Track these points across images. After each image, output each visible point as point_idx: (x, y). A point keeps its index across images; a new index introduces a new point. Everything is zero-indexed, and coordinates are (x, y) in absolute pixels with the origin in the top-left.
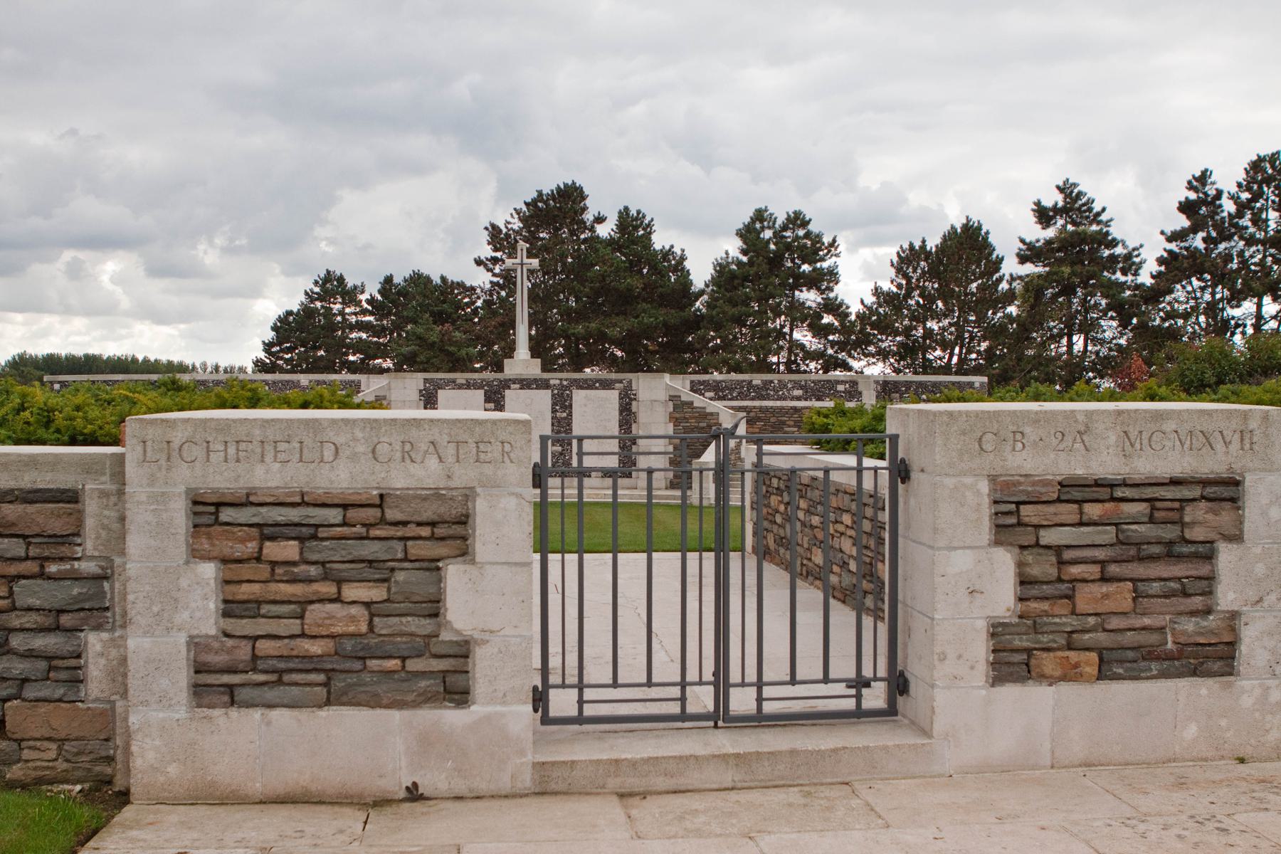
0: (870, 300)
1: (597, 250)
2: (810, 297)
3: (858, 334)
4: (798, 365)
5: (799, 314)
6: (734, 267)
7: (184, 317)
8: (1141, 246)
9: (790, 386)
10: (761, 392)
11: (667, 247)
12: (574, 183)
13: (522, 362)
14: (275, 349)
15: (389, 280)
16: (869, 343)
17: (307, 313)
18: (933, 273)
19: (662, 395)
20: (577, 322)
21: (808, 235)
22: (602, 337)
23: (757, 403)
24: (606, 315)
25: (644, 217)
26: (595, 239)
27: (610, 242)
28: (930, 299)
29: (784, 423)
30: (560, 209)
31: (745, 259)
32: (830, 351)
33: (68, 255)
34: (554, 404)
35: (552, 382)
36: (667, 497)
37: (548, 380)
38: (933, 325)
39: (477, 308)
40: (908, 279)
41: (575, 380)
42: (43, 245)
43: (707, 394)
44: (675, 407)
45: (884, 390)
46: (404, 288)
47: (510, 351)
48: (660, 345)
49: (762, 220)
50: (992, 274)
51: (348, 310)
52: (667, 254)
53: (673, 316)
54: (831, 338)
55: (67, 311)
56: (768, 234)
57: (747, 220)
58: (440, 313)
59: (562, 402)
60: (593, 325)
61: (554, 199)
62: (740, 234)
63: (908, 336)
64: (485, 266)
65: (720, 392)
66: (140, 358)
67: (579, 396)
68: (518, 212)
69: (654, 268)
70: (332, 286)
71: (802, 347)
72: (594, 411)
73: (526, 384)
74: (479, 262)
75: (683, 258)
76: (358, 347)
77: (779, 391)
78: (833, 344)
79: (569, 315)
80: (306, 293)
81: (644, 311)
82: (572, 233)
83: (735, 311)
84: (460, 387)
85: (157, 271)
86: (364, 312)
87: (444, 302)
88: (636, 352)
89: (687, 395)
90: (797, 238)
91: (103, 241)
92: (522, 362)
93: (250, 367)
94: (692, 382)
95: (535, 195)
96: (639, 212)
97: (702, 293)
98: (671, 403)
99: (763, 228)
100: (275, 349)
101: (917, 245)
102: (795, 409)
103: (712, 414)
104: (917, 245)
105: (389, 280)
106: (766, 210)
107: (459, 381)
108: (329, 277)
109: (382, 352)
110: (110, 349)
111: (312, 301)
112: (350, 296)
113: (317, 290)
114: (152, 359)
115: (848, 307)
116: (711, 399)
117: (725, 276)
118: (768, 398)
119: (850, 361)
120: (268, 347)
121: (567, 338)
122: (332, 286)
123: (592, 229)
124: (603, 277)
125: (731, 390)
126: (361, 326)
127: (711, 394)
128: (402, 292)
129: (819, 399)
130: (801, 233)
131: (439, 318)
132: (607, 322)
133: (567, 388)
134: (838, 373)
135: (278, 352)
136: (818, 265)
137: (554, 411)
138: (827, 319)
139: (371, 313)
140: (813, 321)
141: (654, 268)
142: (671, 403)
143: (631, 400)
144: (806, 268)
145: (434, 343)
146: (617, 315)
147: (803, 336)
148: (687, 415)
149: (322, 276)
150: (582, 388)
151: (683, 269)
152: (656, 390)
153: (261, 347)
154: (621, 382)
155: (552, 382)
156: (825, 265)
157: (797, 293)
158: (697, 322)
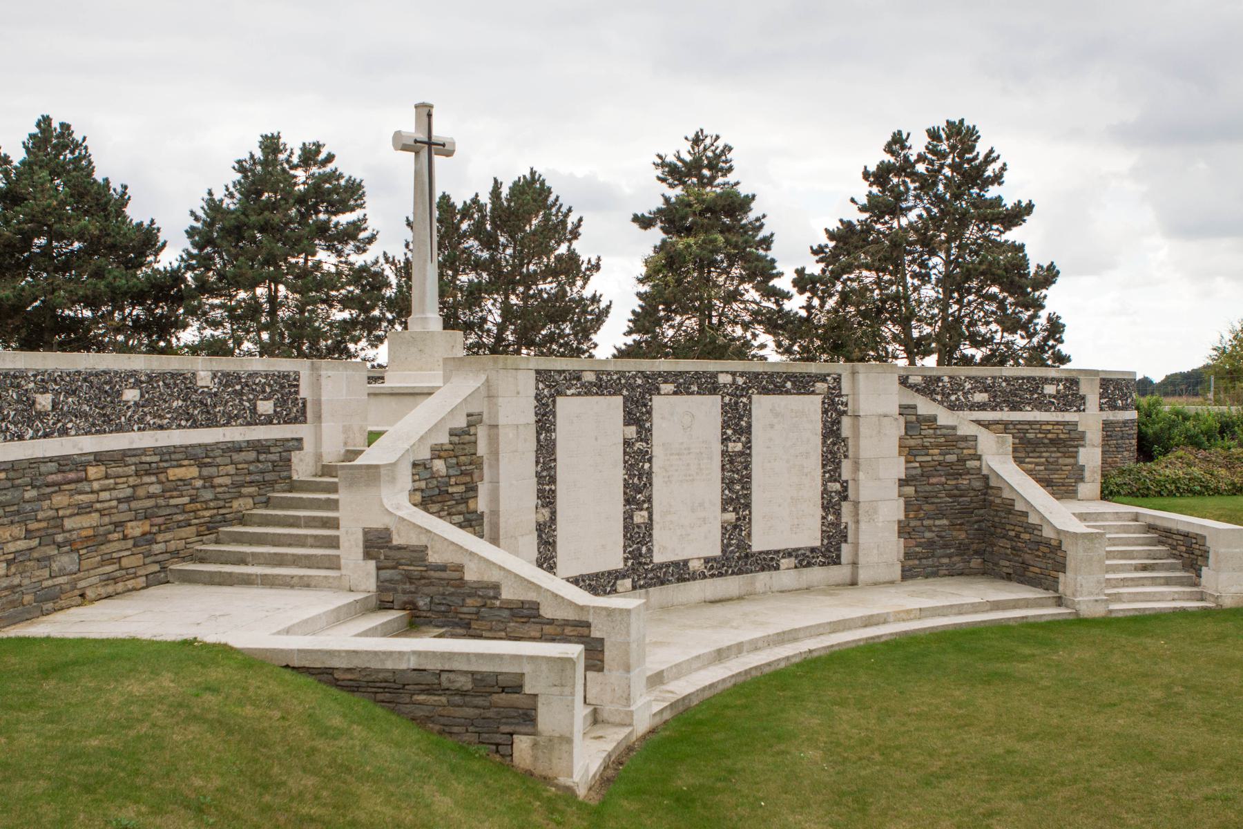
8: (764, 216)
9: (968, 386)
34: (725, 425)
103: (965, 438)
129: (1014, 407)
133: (743, 391)
137: (725, 440)
142: (902, 420)
148: (927, 442)
150: (765, 391)
154: (823, 378)
155: (724, 379)
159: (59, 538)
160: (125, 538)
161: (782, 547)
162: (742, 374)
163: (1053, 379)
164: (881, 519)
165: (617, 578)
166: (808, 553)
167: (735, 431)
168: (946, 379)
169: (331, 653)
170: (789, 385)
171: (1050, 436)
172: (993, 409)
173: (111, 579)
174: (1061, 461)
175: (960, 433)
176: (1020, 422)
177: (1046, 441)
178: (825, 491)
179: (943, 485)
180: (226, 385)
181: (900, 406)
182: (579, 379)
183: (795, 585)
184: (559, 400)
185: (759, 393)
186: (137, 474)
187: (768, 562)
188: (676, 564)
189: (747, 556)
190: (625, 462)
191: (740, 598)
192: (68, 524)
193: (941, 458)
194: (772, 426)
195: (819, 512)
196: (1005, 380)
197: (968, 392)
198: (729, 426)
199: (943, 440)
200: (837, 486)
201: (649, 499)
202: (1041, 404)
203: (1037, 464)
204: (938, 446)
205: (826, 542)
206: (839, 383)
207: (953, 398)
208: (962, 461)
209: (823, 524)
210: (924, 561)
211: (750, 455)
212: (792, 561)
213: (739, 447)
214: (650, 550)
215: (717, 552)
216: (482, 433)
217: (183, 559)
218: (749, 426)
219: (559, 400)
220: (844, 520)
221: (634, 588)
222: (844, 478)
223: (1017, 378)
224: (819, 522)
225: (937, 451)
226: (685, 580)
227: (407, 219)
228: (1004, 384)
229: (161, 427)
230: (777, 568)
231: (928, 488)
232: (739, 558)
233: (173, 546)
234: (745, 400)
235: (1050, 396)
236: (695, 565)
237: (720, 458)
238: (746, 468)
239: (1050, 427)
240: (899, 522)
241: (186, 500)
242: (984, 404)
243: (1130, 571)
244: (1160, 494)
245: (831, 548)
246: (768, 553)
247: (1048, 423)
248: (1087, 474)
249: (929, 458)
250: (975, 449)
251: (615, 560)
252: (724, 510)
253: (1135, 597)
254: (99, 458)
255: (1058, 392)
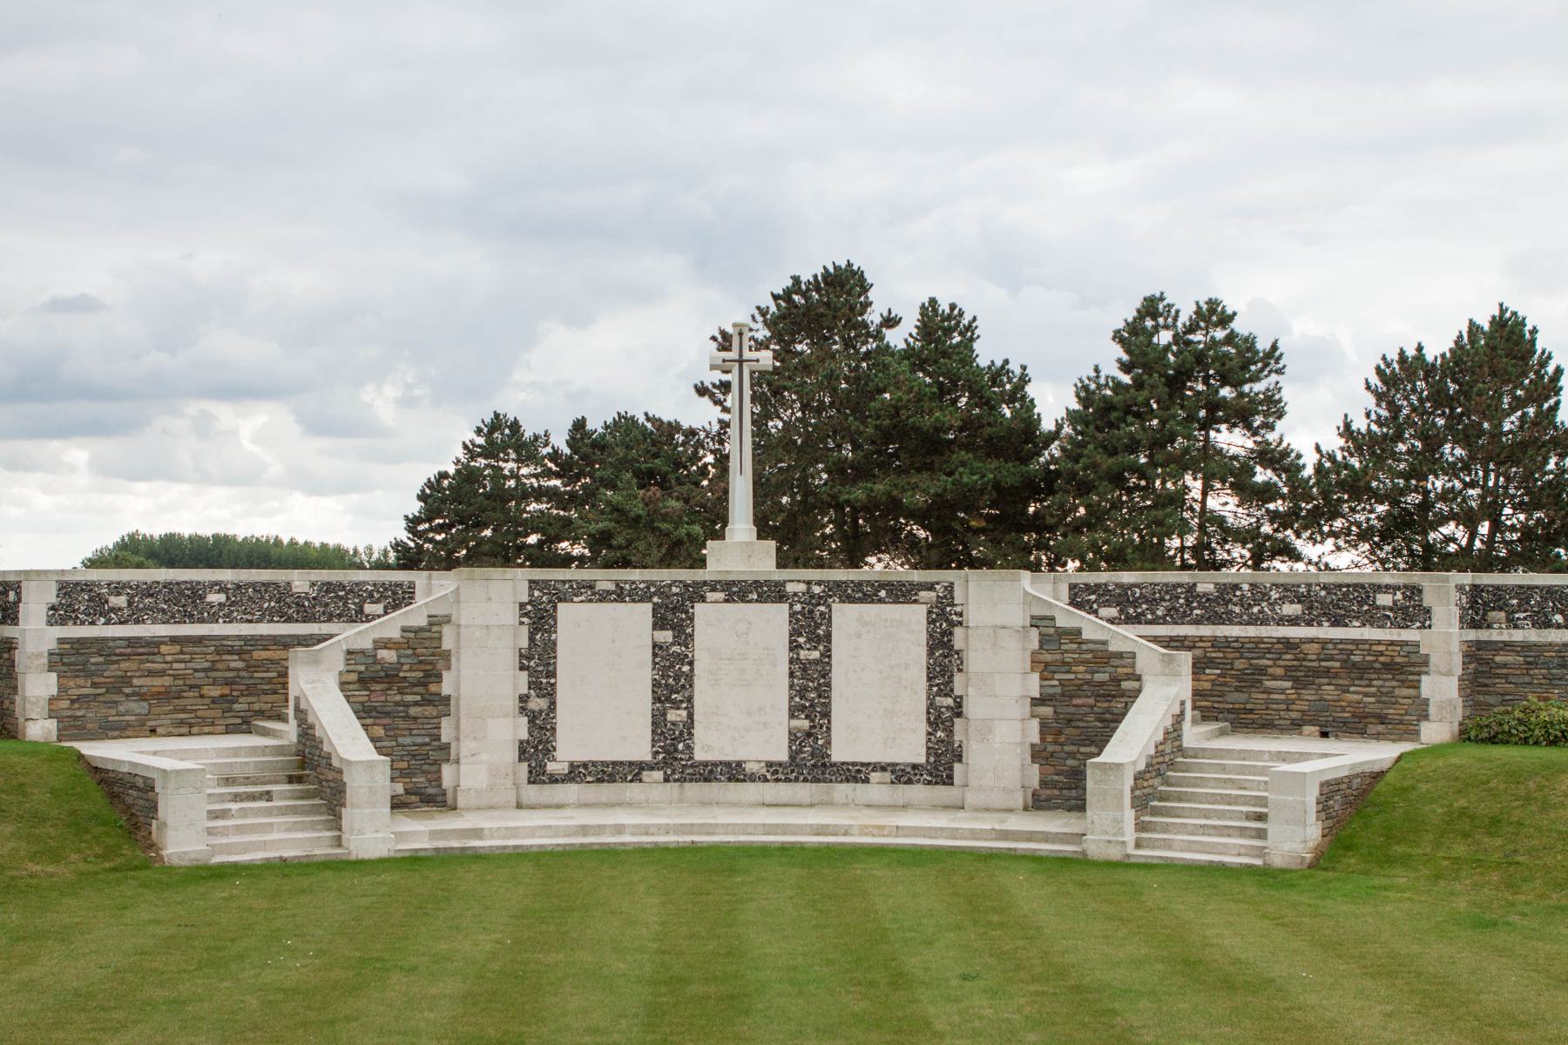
0: (1334, 443)
1: (886, 367)
2: (1232, 440)
3: (1320, 499)
4: (1213, 552)
5: (1217, 469)
6: (1109, 392)
7: (344, 487)
9: (1274, 595)
10: (1218, 607)
11: (999, 363)
12: (849, 264)
13: (741, 549)
14: (421, 528)
15: (579, 425)
16: (1335, 514)
17: (467, 476)
18: (1439, 398)
19: (1018, 617)
20: (854, 482)
21: (1231, 338)
22: (894, 507)
23: (1206, 630)
24: (900, 471)
25: (961, 314)
26: (886, 350)
27: (909, 353)
28: (1432, 442)
29: (1263, 671)
30: (828, 305)
31: (1126, 379)
32: (1267, 529)
33: (193, 408)
34: (794, 633)
35: (790, 588)
36: (1031, 836)
37: (783, 584)
38: (1437, 484)
39: (706, 465)
40: (1395, 409)
41: (838, 584)
42: (164, 392)
43: (1104, 612)
44: (1044, 640)
45: (1473, 603)
46: (602, 436)
47: (715, 519)
48: (988, 518)
49: (1154, 315)
50: (1547, 398)
51: (524, 471)
52: (999, 373)
53: (1010, 473)
54: (1271, 506)
55: (204, 479)
56: (1165, 337)
57: (1131, 315)
58: (651, 474)
59: (811, 628)
60: (880, 487)
61: (818, 289)
62: (1117, 336)
63: (1395, 503)
64: (712, 396)
65: (1130, 607)
66: (286, 541)
67: (845, 616)
68: (763, 312)
69: (980, 397)
70: (502, 436)
71: (1220, 521)
72: (877, 648)
73: (737, 591)
74: (702, 391)
75: (1024, 380)
76: (532, 525)
77: (1254, 606)
78: (1274, 516)
79: (842, 471)
80: (465, 447)
81: (963, 464)
82: (848, 343)
83: (1107, 462)
84: (604, 597)
85: (316, 426)
86: (548, 474)
87: (656, 456)
88: (948, 530)
89: (1068, 617)
90: (1214, 343)
91: (242, 390)
92: (741, 549)
93: (79, 566)
94: (1072, 587)
95: (789, 283)
96: (953, 307)
97: (1055, 436)
98: (1034, 633)
99: (1156, 328)
100: (421, 528)
101: (1411, 352)
102: (1288, 644)
103: (1120, 655)
104: (1411, 352)
105: (579, 425)
106: (1162, 299)
107: (600, 586)
108: (497, 423)
109: (565, 529)
110: (246, 526)
111: (472, 458)
112: (526, 450)
113: (480, 441)
114: (301, 541)
115: (1299, 456)
116: (1111, 621)
117: (1100, 411)
118: (1228, 619)
119: (1299, 544)
120: (412, 523)
121: (839, 507)
122: (502, 436)
123: (878, 336)
124: (896, 409)
125: (1153, 603)
126: (539, 494)
127: (1113, 612)
128: (600, 445)
129: (1337, 622)
130: (1220, 334)
131: (646, 478)
132: (902, 481)
133: (822, 599)
134: (1281, 566)
135: (426, 531)
136: (1246, 388)
137: (794, 647)
138: (1262, 475)
139: (558, 475)
140: (1238, 477)
141: (980, 397)
142: (1034, 633)
143: (952, 624)
144: (1226, 392)
145: (639, 517)
146: (919, 471)
147: (1224, 503)
148: (1068, 658)
149: (488, 421)
150: (850, 599)
151: (1024, 397)
152: (1004, 605)
153: (403, 524)
154: (930, 587)
155: (790, 588)
156: (1259, 387)
157: (1212, 434)
158: (1047, 483)
159: (127, 690)
160: (202, 696)
161: (873, 760)
162: (819, 583)
163: (1388, 587)
164: (998, 739)
165: (642, 769)
166: (909, 769)
167: (809, 640)
168: (1246, 587)
169: (107, 760)
170: (883, 593)
171: (1382, 659)
172: (1309, 624)
173: (182, 723)
174: (1397, 692)
175: (1111, 648)
176: (1342, 641)
177: (1377, 665)
178: (931, 705)
179: (1092, 707)
180: (327, 591)
181: (1033, 617)
182: (591, 587)
183: (887, 800)
184: (560, 606)
185: (842, 601)
186: (218, 654)
187: (856, 773)
188: (728, 764)
189: (824, 765)
190: (654, 663)
191: (811, 805)
192: (136, 681)
193: (1088, 676)
194: (859, 636)
195: (923, 727)
196: (1325, 588)
197: (1275, 602)
198: (800, 635)
199: (1090, 656)
200: (949, 701)
201: (690, 700)
202: (1373, 617)
203: (1366, 695)
204: (1083, 662)
205: (932, 759)
206: (951, 592)
207: (1255, 610)
208: (1116, 681)
209: (929, 740)
210: (1066, 792)
211: (829, 664)
212: (888, 776)
213: (816, 655)
214: (689, 748)
215: (784, 756)
216: (447, 631)
217: (270, 718)
218: (828, 636)
219: (560, 606)
220: (956, 738)
221: (666, 780)
222: (957, 692)
223: (1340, 586)
224: (924, 739)
225: (1082, 668)
226: (738, 780)
227: (1367, 382)
228: (1323, 593)
229: (250, 621)
230: (867, 781)
231: (1072, 710)
232: (814, 766)
233: (257, 707)
234: (822, 608)
235: (1384, 608)
236: (750, 767)
237: (787, 666)
238: (824, 676)
239: (1382, 648)
240: (1033, 745)
241: (274, 674)
242: (1297, 618)
243: (1240, 819)
244: (1525, 741)
245: (941, 764)
246: (854, 764)
247: (1379, 642)
248: (1432, 710)
249: (1072, 676)
250: (1133, 666)
251: (640, 748)
252: (792, 716)
253: (1190, 846)
254: (174, 640)
255: (1395, 602)
